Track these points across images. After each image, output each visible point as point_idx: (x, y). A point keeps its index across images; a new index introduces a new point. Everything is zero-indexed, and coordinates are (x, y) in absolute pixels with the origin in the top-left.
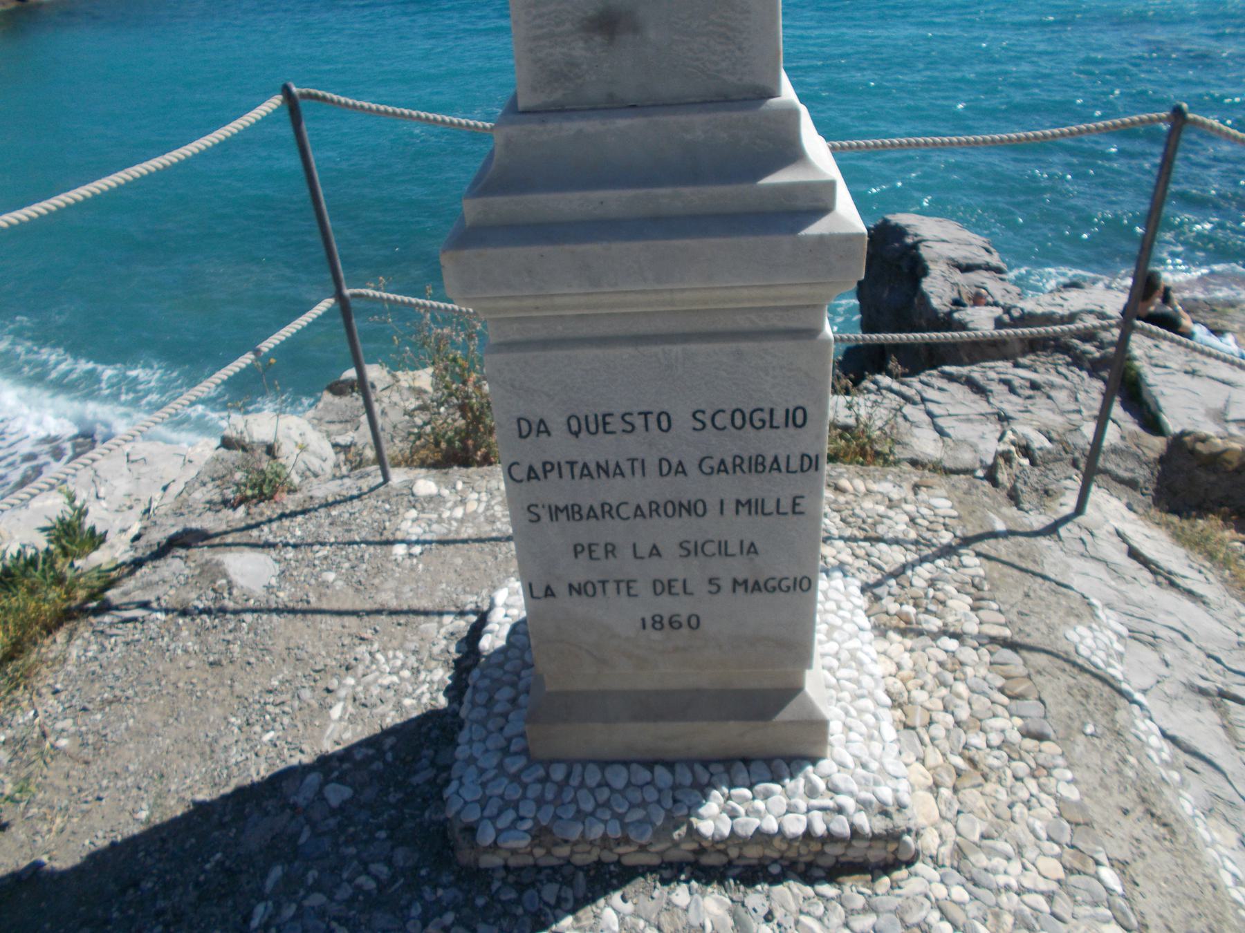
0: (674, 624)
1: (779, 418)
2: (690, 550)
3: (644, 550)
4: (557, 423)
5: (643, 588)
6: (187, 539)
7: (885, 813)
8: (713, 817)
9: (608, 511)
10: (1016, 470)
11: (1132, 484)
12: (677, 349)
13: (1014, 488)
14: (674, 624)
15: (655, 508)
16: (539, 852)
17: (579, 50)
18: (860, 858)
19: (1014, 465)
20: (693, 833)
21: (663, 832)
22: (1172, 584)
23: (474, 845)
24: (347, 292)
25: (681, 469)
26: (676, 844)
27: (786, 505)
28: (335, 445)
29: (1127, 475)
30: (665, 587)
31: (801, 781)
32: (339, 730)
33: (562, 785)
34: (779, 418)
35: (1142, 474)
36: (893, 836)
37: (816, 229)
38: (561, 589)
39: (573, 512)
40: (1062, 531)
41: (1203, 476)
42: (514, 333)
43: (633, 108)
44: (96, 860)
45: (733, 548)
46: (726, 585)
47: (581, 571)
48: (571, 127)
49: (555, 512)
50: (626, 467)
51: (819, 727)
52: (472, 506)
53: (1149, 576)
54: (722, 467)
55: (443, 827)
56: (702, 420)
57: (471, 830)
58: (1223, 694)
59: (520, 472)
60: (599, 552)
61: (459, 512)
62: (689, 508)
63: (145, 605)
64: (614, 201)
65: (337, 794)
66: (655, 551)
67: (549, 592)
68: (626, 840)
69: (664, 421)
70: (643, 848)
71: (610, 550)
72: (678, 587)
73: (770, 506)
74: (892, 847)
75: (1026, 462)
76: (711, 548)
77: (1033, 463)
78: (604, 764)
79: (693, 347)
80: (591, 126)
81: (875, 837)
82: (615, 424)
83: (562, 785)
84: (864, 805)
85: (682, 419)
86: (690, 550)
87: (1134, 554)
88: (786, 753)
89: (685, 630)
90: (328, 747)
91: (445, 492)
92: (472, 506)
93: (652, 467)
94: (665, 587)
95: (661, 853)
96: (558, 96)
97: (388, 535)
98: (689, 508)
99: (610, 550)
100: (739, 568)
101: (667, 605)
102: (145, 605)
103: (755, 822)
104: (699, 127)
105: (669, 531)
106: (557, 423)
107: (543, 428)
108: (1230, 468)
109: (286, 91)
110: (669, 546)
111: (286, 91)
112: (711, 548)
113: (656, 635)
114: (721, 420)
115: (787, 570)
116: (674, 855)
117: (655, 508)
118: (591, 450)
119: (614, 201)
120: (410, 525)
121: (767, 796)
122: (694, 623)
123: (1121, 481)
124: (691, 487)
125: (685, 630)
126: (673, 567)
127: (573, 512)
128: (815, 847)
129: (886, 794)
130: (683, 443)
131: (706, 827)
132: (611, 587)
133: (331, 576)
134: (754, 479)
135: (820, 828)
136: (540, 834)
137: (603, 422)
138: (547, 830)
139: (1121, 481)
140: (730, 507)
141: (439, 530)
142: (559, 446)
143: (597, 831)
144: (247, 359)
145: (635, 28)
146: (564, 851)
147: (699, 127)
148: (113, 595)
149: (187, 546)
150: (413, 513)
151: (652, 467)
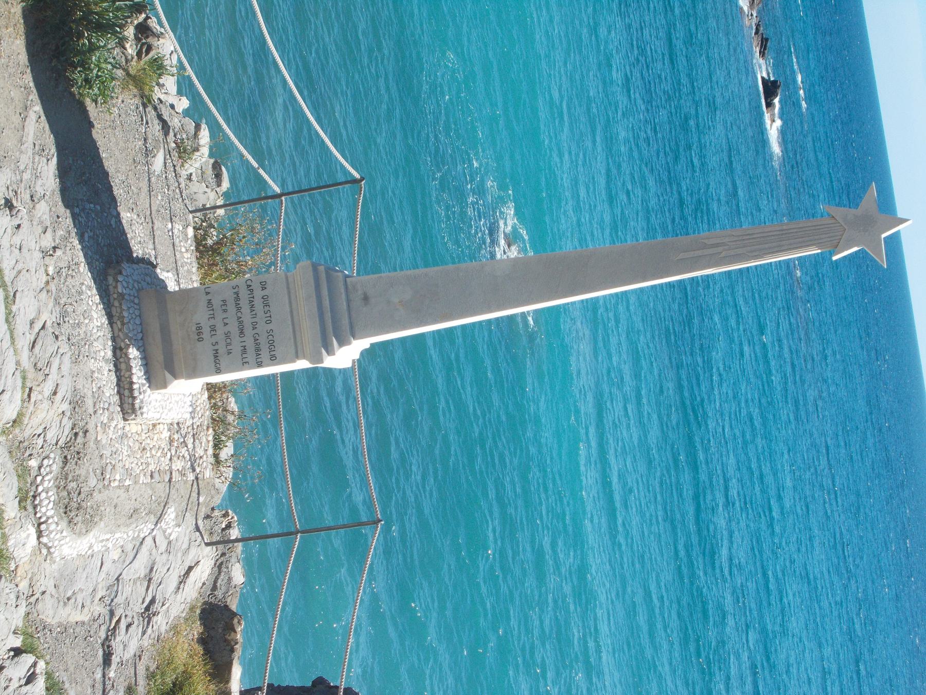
0: (199, 334)
1: (272, 353)
2: (227, 335)
3: (225, 321)
4: (265, 292)
5: (212, 322)
6: (166, 129)
7: (140, 408)
8: (133, 352)
9: (239, 309)
11: (214, 588)
12: (290, 323)
14: (199, 334)
15: (241, 323)
16: (115, 296)
17: (360, 292)
18: (127, 403)
20: (128, 346)
21: (126, 336)
22: (181, 583)
23: (116, 274)
24: (283, 198)
26: (123, 341)
27: (245, 360)
28: (191, 174)
29: (218, 585)
30: (213, 329)
31: (144, 382)
32: (126, 216)
33: (133, 302)
34: (272, 353)
35: (219, 593)
36: (134, 411)
37: (323, 351)
38: (209, 297)
39: (237, 298)
40: (198, 533)
41: (221, 625)
42: (290, 280)
43: (349, 306)
44: (94, 142)
45: (229, 347)
46: (216, 347)
47: (217, 302)
48: (343, 291)
49: (237, 293)
51: (165, 386)
52: (186, 255)
53: (182, 574)
54: (256, 340)
55: (118, 262)
56: (270, 333)
57: (121, 273)
58: (150, 580)
59: (249, 283)
60: (224, 308)
61: (183, 250)
62: (242, 332)
63: (147, 123)
64: (326, 303)
65: (113, 222)
68: (123, 324)
69: (269, 322)
70: (120, 330)
71: (225, 311)
72: (213, 333)
73: (244, 356)
74: (130, 411)
75: (224, 526)
76: (228, 341)
77: (223, 530)
78: (140, 316)
79: (291, 327)
80: (344, 296)
81: (133, 405)
82: (267, 308)
83: (133, 302)
84: (142, 402)
85: (270, 327)
86: (227, 335)
87: (190, 569)
88: (155, 380)
89: (197, 337)
90: (122, 215)
91: (189, 242)
92: (186, 255)
93: (254, 320)
94: (213, 329)
95: (118, 336)
96: (350, 287)
97: (174, 218)
98: (242, 332)
99: (225, 311)
100: (222, 349)
101: (206, 330)
102: (147, 123)
103: (134, 366)
104: (345, 322)
105: (233, 328)
106: (265, 292)
107: (264, 288)
109: (362, 179)
110: (227, 328)
111: (362, 179)
112: (228, 341)
113: (194, 329)
114: (271, 337)
115: (222, 366)
116: (118, 340)
117: (241, 323)
118: (258, 303)
119: (326, 303)
120: (178, 227)
121: (140, 370)
122: (200, 340)
123: (215, 582)
124: (249, 332)
125: (197, 337)
126: (221, 330)
127: (237, 298)
128: (127, 386)
129: (145, 410)
130: (262, 328)
131: (130, 350)
132: (212, 312)
133: (160, 198)
134: (253, 349)
135: (135, 386)
136: (122, 296)
137: (267, 305)
138: (123, 298)
139: (215, 582)
140: (244, 344)
141: (177, 241)
142: (258, 293)
143: (125, 314)
144: (255, 165)
145: (366, 304)
146: (116, 304)
147: (345, 322)
148: (149, 109)
149: (163, 128)
150: (181, 228)
151: (254, 320)
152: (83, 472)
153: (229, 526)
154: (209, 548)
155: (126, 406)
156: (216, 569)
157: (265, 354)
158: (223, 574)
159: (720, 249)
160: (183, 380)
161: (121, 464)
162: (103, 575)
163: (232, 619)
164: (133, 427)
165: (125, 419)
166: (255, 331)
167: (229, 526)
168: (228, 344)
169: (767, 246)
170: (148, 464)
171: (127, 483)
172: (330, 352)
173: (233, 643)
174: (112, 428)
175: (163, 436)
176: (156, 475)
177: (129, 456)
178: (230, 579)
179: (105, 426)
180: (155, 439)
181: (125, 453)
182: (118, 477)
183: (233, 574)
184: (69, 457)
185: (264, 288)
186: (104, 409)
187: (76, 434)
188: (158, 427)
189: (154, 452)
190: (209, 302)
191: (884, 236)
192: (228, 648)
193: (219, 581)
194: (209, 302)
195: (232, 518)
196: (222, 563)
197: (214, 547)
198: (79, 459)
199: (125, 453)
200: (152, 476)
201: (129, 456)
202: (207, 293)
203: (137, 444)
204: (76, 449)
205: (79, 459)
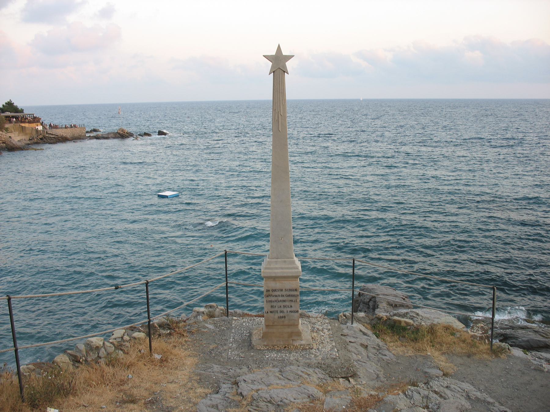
39: (271, 301)
171: (336, 350)
178: (363, 317)
190: (271, 312)
194: (271, 312)
200: (332, 341)
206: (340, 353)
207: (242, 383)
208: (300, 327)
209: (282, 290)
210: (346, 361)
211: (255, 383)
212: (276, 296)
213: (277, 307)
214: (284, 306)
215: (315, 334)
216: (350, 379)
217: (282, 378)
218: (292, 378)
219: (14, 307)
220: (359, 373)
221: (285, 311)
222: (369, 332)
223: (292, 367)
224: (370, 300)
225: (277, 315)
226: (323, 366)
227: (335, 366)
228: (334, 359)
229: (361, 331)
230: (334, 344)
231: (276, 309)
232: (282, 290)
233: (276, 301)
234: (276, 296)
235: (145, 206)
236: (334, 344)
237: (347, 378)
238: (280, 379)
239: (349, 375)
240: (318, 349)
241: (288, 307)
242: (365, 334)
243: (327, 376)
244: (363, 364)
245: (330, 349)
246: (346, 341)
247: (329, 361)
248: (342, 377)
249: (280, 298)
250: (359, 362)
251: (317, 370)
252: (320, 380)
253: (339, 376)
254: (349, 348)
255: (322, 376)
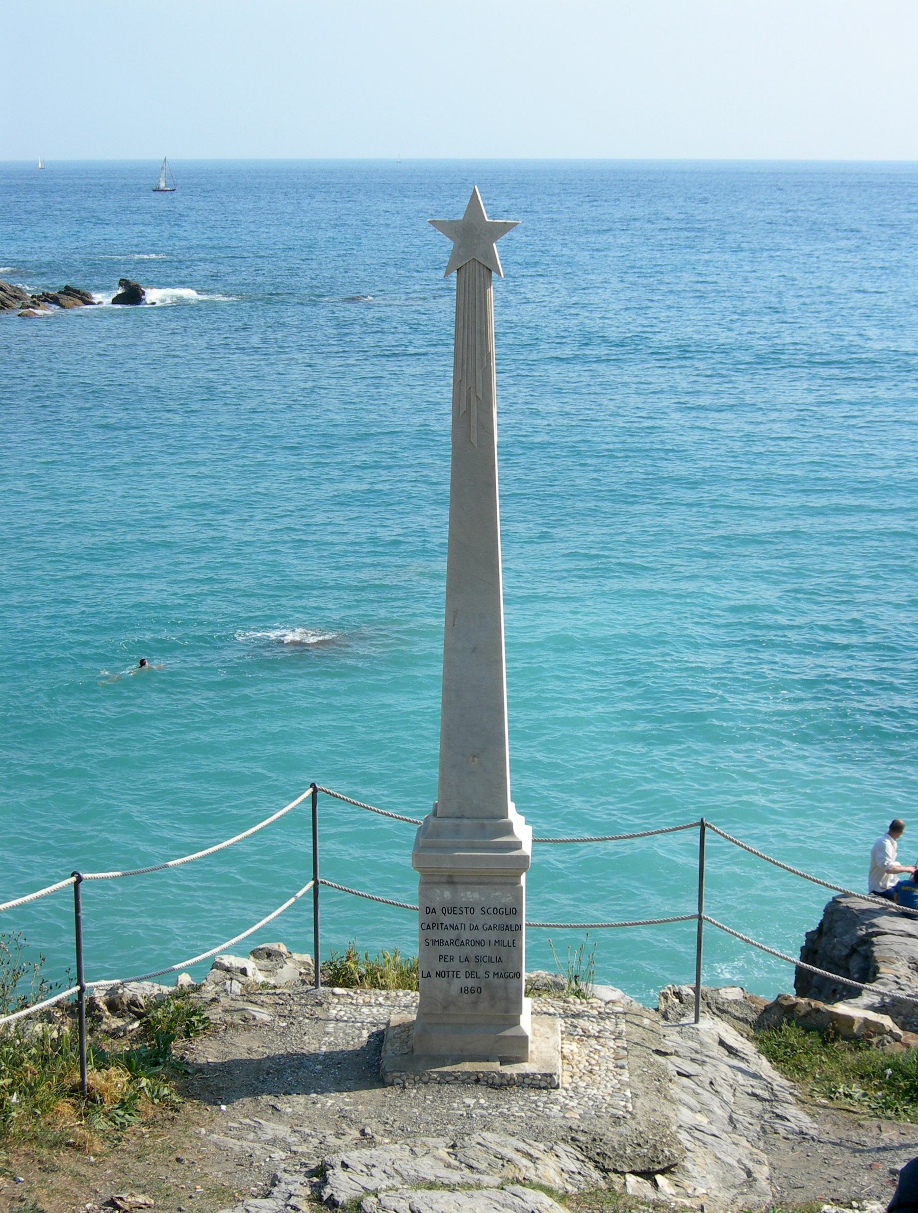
5: (462, 974)
10: (670, 1003)
13: (666, 1012)
19: (669, 1001)
25: (477, 928)
29: (741, 1016)
38: (433, 974)
39: (440, 942)
47: (441, 967)
50: (459, 926)
54: (490, 928)
66: (467, 960)
67: (429, 975)
71: (452, 959)
73: (506, 944)
75: (677, 1001)
76: (486, 959)
77: (681, 1002)
82: (457, 911)
108: (800, 1014)
109: (313, 785)
111: (313, 785)
113: (466, 996)
123: (738, 1018)
139: (738, 1018)
144: (293, 900)
152: (616, 1138)
153: (678, 995)
154: (701, 1019)
155: (543, 1084)
156: (723, 1016)
157: (511, 920)
158: (730, 1009)
159: (473, 398)
160: (521, 1017)
161: (608, 1098)
162: (724, 1136)
163: (782, 1006)
164: (564, 1079)
165: (557, 1087)
166: (480, 927)
167: (678, 995)
168: (490, 960)
169: (478, 347)
170: (608, 1070)
171: (628, 1093)
172: (518, 845)
173: (809, 1009)
174: (567, 1102)
175: (576, 1050)
176: (620, 1063)
177: (598, 1088)
178: (736, 1002)
179: (564, 1108)
180: (579, 1059)
181: (595, 1091)
182: (623, 1103)
183: (730, 998)
184: (598, 1151)
185: (434, 911)
186: (544, 1107)
187: (573, 1139)
188: (565, 1054)
189: (593, 1062)
190: (439, 974)
191: (487, 220)
192: (814, 1015)
193: (737, 1014)
194: (439, 974)
195: (669, 989)
196: (718, 1009)
197: (701, 1014)
198: (601, 1140)
199: (595, 1091)
200: (622, 1067)
201: (598, 1088)
202: (429, 975)
203: (585, 1078)
204: (590, 1142)
205: (601, 1140)
206: (638, 1103)
207: (339, 1170)
208: (526, 1022)
209: (472, 910)
210: (653, 1126)
211: (373, 1171)
212: (454, 927)
213: (456, 960)
214: (478, 960)
215: (574, 1046)
216: (659, 1177)
217: (457, 1163)
218: (483, 1166)
219: (414, 935)
220: (688, 1164)
221: (481, 973)
222: (748, 1048)
223: (487, 1135)
224: (853, 951)
225: (457, 984)
226: (582, 1138)
227: (616, 1138)
228: (617, 1120)
229: (722, 1043)
230: (625, 1077)
231: (455, 965)
232: (472, 910)
233: (453, 942)
234: (454, 927)
235: (583, 1161)
236: (625, 1077)
237: (648, 1175)
238: (449, 1166)
239: (658, 1167)
240: (575, 1089)
241: (490, 960)
242: (732, 1051)
243: (591, 1165)
244: (709, 1139)
245: (610, 1090)
246: (665, 1071)
247: (603, 1126)
248: (633, 1173)
249: (466, 935)
250: (697, 1134)
251: (561, 1148)
252: (566, 1176)
253: (626, 1169)
254: (674, 1090)
255: (573, 1166)
